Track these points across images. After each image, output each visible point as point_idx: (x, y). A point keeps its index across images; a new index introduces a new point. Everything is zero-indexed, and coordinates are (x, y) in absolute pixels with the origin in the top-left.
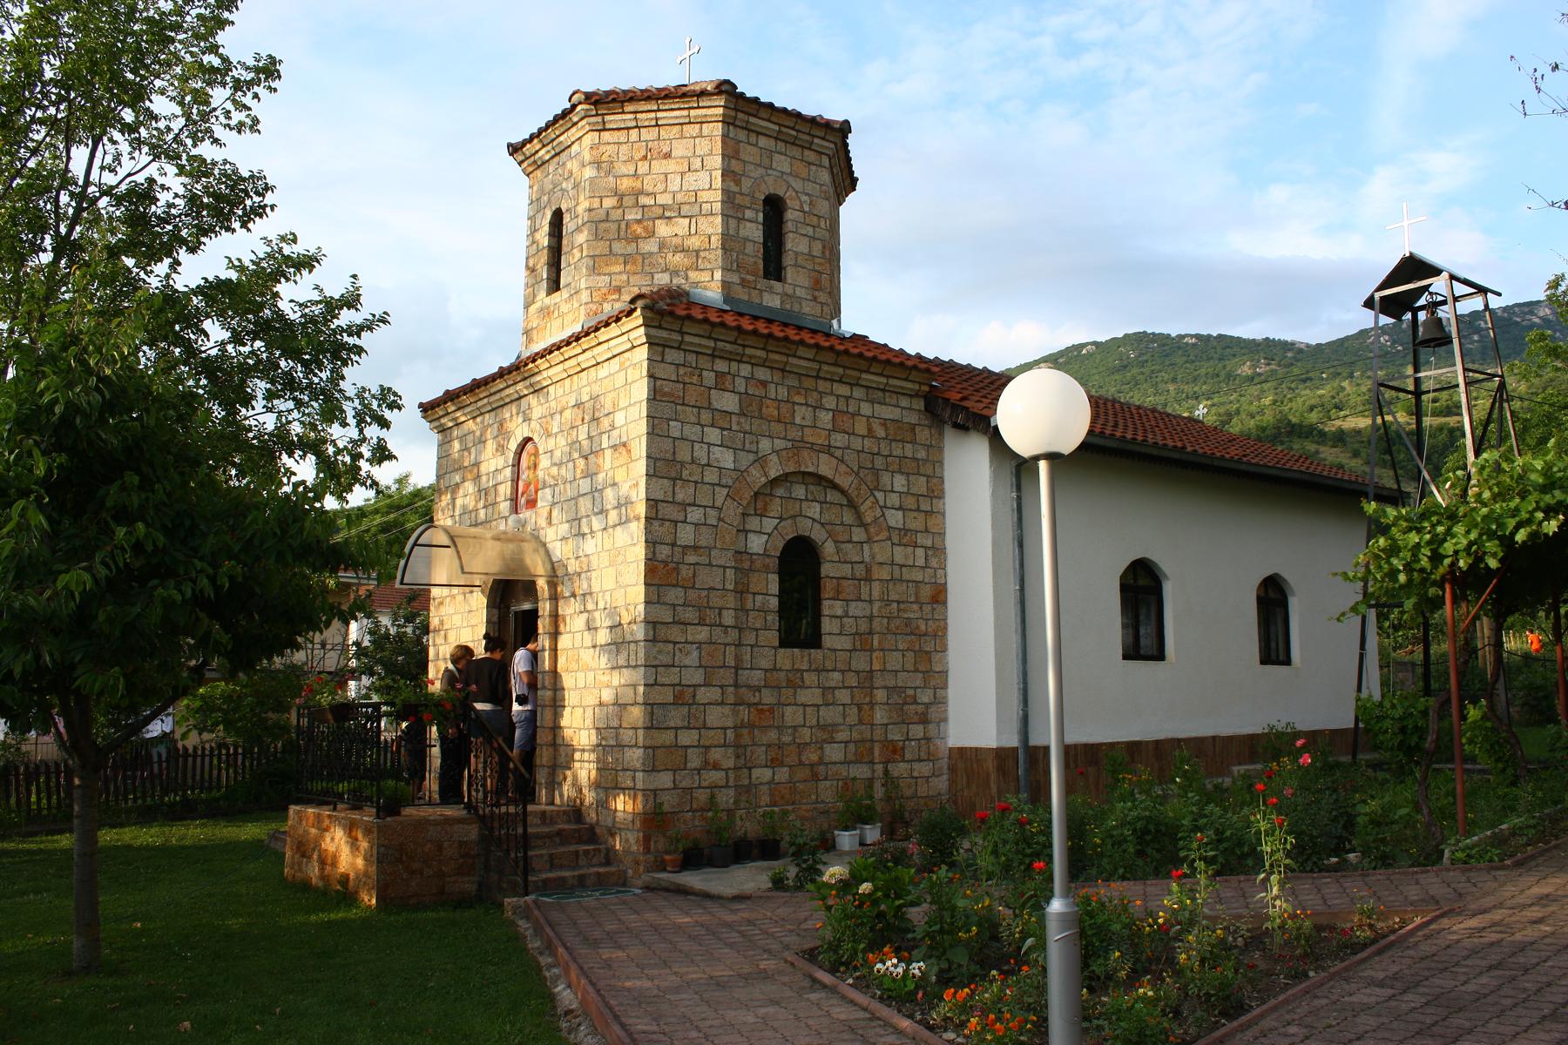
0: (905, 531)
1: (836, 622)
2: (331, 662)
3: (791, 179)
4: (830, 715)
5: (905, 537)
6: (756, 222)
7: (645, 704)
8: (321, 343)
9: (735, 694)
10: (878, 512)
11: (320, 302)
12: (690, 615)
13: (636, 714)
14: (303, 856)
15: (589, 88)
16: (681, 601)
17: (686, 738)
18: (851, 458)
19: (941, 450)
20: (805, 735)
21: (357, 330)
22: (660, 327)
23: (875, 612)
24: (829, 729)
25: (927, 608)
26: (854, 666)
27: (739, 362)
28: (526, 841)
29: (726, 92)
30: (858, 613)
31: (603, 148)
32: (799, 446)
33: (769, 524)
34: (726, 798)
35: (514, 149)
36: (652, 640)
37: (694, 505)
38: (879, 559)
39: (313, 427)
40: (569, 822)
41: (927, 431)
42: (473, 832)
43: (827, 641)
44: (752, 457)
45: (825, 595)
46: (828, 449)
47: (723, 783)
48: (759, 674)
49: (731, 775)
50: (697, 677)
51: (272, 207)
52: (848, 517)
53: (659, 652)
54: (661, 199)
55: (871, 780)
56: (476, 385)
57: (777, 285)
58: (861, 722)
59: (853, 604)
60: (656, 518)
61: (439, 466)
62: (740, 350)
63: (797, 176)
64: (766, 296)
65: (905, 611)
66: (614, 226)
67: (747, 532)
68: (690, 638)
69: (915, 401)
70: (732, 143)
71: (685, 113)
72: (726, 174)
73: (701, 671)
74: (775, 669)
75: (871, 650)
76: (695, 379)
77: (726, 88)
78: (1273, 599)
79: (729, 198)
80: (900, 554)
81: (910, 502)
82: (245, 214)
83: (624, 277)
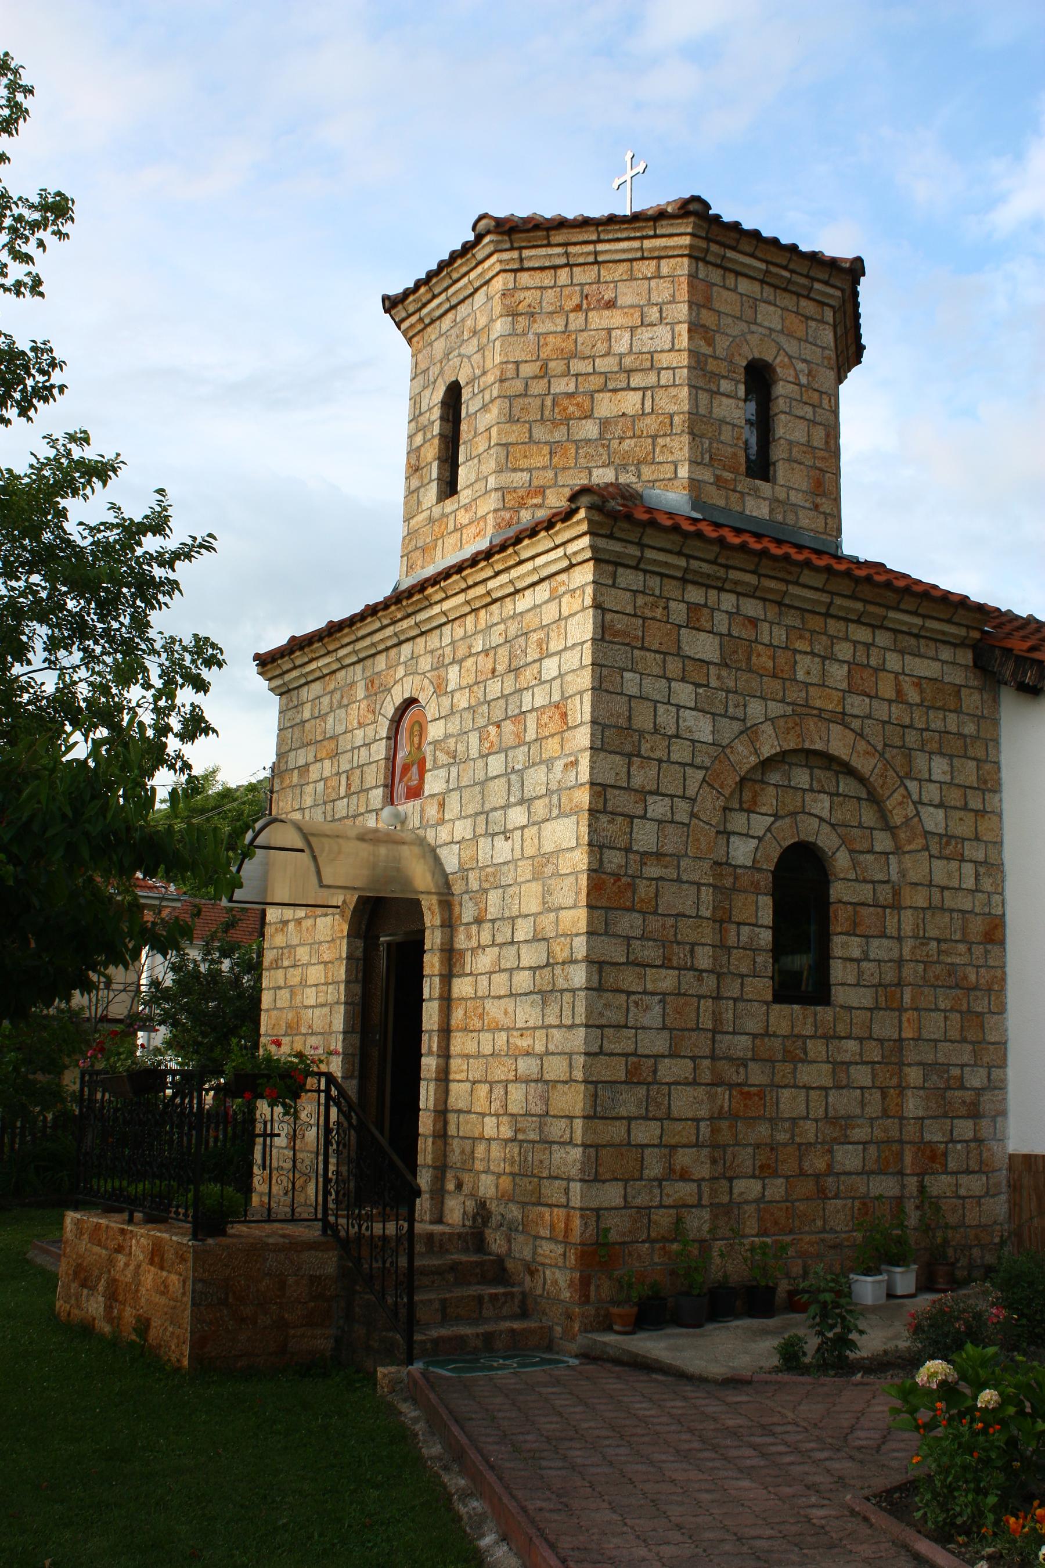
0: (947, 838)
1: (852, 967)
2: (119, 1009)
3: (782, 340)
4: (843, 1102)
5: (948, 847)
6: (735, 397)
7: (586, 1082)
8: (119, 578)
9: (713, 1071)
10: (911, 811)
11: (117, 526)
12: (650, 952)
13: (572, 1100)
14: (84, 1285)
15: (500, 212)
16: (638, 933)
17: (645, 1133)
18: (872, 730)
19: (996, 723)
20: (809, 1131)
21: (168, 561)
22: (611, 536)
23: (907, 953)
24: (840, 1123)
25: (978, 951)
26: (877, 1031)
27: (721, 589)
28: (409, 1281)
29: (695, 214)
30: (883, 955)
31: (520, 295)
32: (802, 712)
33: (760, 823)
34: (698, 1222)
35: (391, 304)
36: (597, 988)
37: (656, 793)
38: (913, 876)
39: (105, 690)
40: (466, 1250)
41: (976, 696)
42: (329, 1263)
43: (839, 995)
44: (737, 726)
45: (836, 927)
46: (842, 718)
47: (694, 1200)
48: (744, 1041)
49: (706, 1189)
50: (659, 1043)
51: (62, 388)
52: (869, 817)
53: (607, 1006)
55: (900, 1200)
56: (334, 629)
57: (764, 487)
58: (885, 1114)
59: (875, 942)
60: (605, 812)
61: (279, 745)
62: (721, 572)
63: (790, 335)
65: (947, 953)
67: (729, 834)
68: (650, 987)
69: (960, 652)
70: (701, 286)
71: (636, 244)
72: (695, 328)
73: (665, 1034)
74: (767, 1034)
75: (901, 1010)
76: (659, 613)
77: (694, 209)
79: (698, 362)
80: (941, 871)
81: (954, 797)
82: (24, 398)
83: (550, 474)
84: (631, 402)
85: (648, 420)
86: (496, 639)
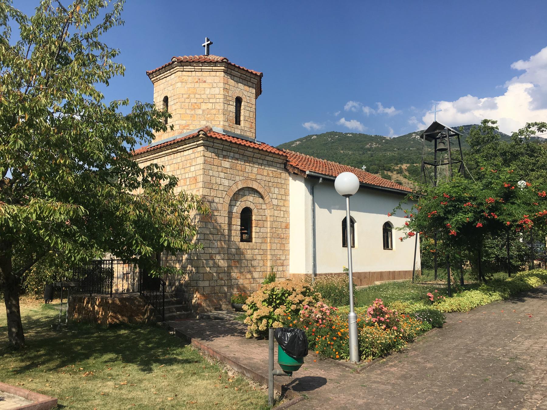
0: (278, 205)
3: (244, 92)
10: (270, 200)
22: (207, 140)
25: (284, 230)
29: (225, 62)
43: (254, 240)
44: (233, 182)
46: (256, 180)
54: (203, 96)
64: (236, 130)
66: (187, 104)
72: (225, 89)
78: (387, 228)
79: (225, 97)
83: (191, 121)
84: (210, 106)
85: (214, 110)
86: (179, 161)
